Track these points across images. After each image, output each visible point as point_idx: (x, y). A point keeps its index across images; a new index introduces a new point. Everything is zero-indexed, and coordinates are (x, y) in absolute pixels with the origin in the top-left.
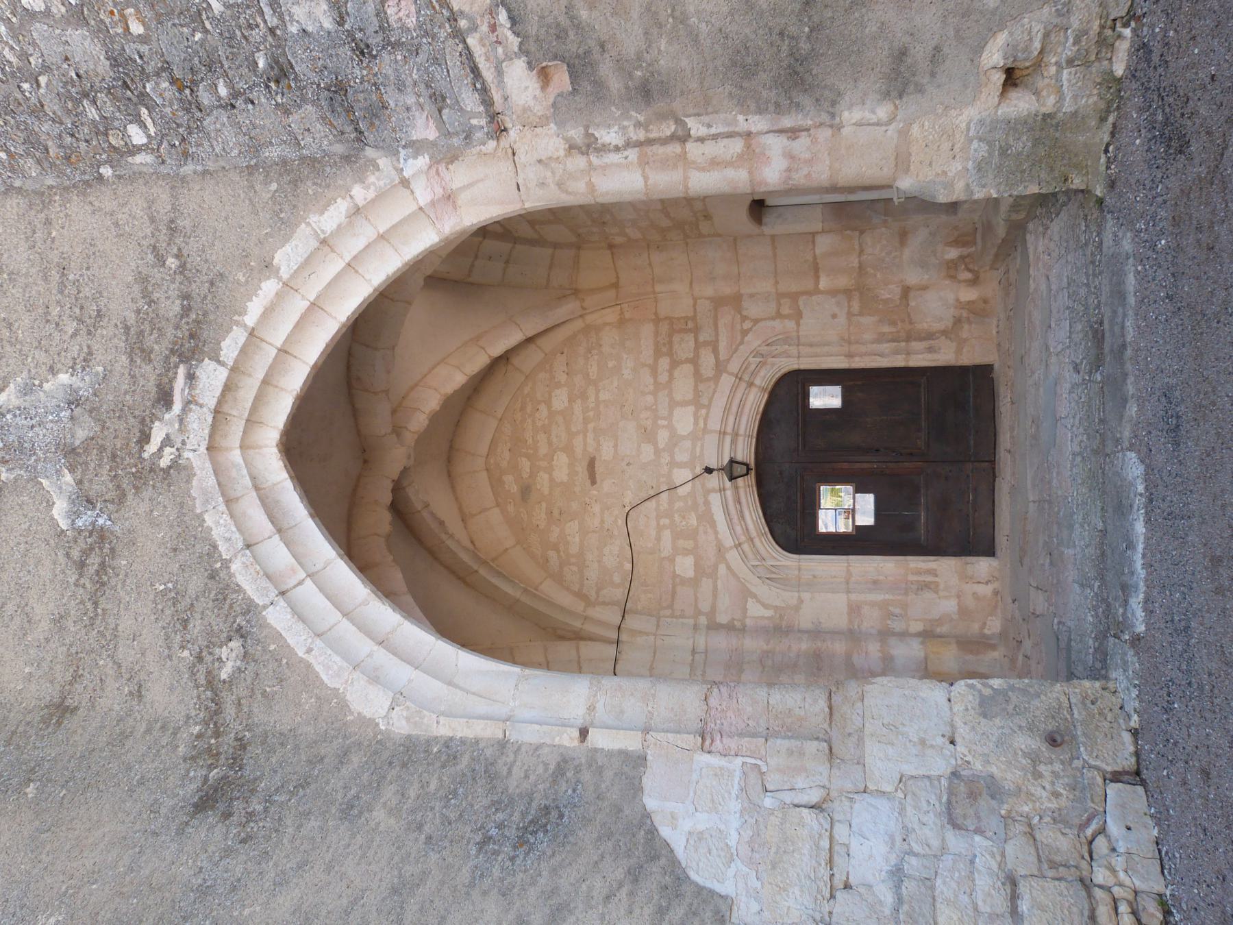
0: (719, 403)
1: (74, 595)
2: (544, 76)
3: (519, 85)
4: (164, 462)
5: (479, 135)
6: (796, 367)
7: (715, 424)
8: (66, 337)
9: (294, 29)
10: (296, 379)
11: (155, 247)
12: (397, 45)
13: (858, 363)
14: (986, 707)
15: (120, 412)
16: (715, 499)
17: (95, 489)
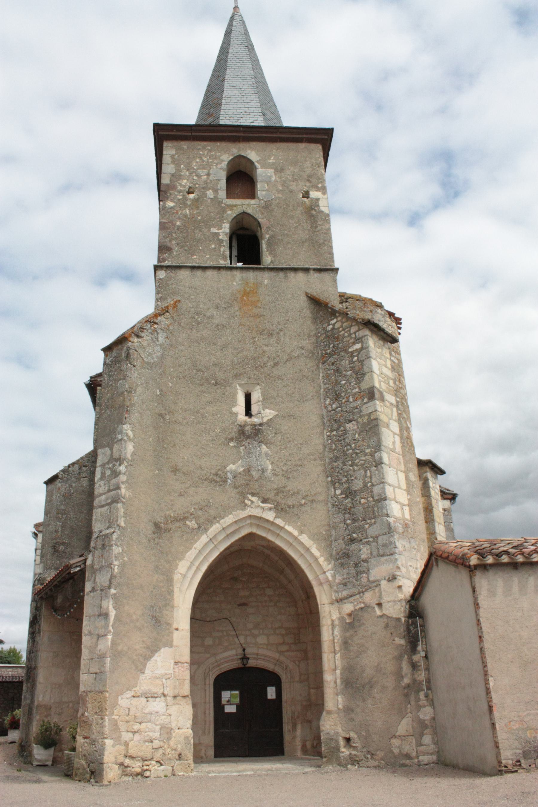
0: (269, 653)
1: (208, 472)
2: (350, 615)
3: (348, 607)
4: (246, 501)
5: (337, 595)
6: (282, 681)
7: (261, 651)
8: (282, 467)
9: (361, 547)
10: (271, 538)
11: (307, 495)
12: (357, 574)
13: (284, 705)
14: (186, 738)
15: (261, 486)
16: (233, 652)
17: (238, 478)
